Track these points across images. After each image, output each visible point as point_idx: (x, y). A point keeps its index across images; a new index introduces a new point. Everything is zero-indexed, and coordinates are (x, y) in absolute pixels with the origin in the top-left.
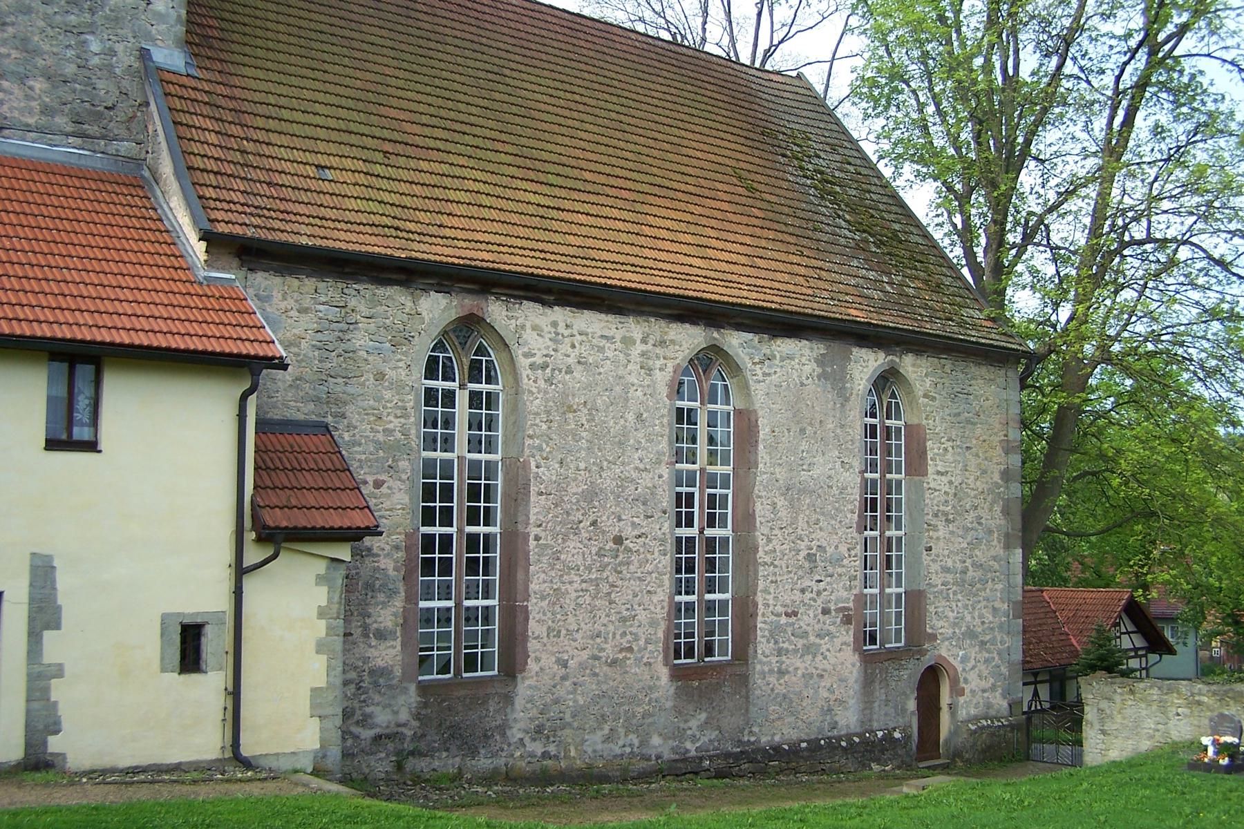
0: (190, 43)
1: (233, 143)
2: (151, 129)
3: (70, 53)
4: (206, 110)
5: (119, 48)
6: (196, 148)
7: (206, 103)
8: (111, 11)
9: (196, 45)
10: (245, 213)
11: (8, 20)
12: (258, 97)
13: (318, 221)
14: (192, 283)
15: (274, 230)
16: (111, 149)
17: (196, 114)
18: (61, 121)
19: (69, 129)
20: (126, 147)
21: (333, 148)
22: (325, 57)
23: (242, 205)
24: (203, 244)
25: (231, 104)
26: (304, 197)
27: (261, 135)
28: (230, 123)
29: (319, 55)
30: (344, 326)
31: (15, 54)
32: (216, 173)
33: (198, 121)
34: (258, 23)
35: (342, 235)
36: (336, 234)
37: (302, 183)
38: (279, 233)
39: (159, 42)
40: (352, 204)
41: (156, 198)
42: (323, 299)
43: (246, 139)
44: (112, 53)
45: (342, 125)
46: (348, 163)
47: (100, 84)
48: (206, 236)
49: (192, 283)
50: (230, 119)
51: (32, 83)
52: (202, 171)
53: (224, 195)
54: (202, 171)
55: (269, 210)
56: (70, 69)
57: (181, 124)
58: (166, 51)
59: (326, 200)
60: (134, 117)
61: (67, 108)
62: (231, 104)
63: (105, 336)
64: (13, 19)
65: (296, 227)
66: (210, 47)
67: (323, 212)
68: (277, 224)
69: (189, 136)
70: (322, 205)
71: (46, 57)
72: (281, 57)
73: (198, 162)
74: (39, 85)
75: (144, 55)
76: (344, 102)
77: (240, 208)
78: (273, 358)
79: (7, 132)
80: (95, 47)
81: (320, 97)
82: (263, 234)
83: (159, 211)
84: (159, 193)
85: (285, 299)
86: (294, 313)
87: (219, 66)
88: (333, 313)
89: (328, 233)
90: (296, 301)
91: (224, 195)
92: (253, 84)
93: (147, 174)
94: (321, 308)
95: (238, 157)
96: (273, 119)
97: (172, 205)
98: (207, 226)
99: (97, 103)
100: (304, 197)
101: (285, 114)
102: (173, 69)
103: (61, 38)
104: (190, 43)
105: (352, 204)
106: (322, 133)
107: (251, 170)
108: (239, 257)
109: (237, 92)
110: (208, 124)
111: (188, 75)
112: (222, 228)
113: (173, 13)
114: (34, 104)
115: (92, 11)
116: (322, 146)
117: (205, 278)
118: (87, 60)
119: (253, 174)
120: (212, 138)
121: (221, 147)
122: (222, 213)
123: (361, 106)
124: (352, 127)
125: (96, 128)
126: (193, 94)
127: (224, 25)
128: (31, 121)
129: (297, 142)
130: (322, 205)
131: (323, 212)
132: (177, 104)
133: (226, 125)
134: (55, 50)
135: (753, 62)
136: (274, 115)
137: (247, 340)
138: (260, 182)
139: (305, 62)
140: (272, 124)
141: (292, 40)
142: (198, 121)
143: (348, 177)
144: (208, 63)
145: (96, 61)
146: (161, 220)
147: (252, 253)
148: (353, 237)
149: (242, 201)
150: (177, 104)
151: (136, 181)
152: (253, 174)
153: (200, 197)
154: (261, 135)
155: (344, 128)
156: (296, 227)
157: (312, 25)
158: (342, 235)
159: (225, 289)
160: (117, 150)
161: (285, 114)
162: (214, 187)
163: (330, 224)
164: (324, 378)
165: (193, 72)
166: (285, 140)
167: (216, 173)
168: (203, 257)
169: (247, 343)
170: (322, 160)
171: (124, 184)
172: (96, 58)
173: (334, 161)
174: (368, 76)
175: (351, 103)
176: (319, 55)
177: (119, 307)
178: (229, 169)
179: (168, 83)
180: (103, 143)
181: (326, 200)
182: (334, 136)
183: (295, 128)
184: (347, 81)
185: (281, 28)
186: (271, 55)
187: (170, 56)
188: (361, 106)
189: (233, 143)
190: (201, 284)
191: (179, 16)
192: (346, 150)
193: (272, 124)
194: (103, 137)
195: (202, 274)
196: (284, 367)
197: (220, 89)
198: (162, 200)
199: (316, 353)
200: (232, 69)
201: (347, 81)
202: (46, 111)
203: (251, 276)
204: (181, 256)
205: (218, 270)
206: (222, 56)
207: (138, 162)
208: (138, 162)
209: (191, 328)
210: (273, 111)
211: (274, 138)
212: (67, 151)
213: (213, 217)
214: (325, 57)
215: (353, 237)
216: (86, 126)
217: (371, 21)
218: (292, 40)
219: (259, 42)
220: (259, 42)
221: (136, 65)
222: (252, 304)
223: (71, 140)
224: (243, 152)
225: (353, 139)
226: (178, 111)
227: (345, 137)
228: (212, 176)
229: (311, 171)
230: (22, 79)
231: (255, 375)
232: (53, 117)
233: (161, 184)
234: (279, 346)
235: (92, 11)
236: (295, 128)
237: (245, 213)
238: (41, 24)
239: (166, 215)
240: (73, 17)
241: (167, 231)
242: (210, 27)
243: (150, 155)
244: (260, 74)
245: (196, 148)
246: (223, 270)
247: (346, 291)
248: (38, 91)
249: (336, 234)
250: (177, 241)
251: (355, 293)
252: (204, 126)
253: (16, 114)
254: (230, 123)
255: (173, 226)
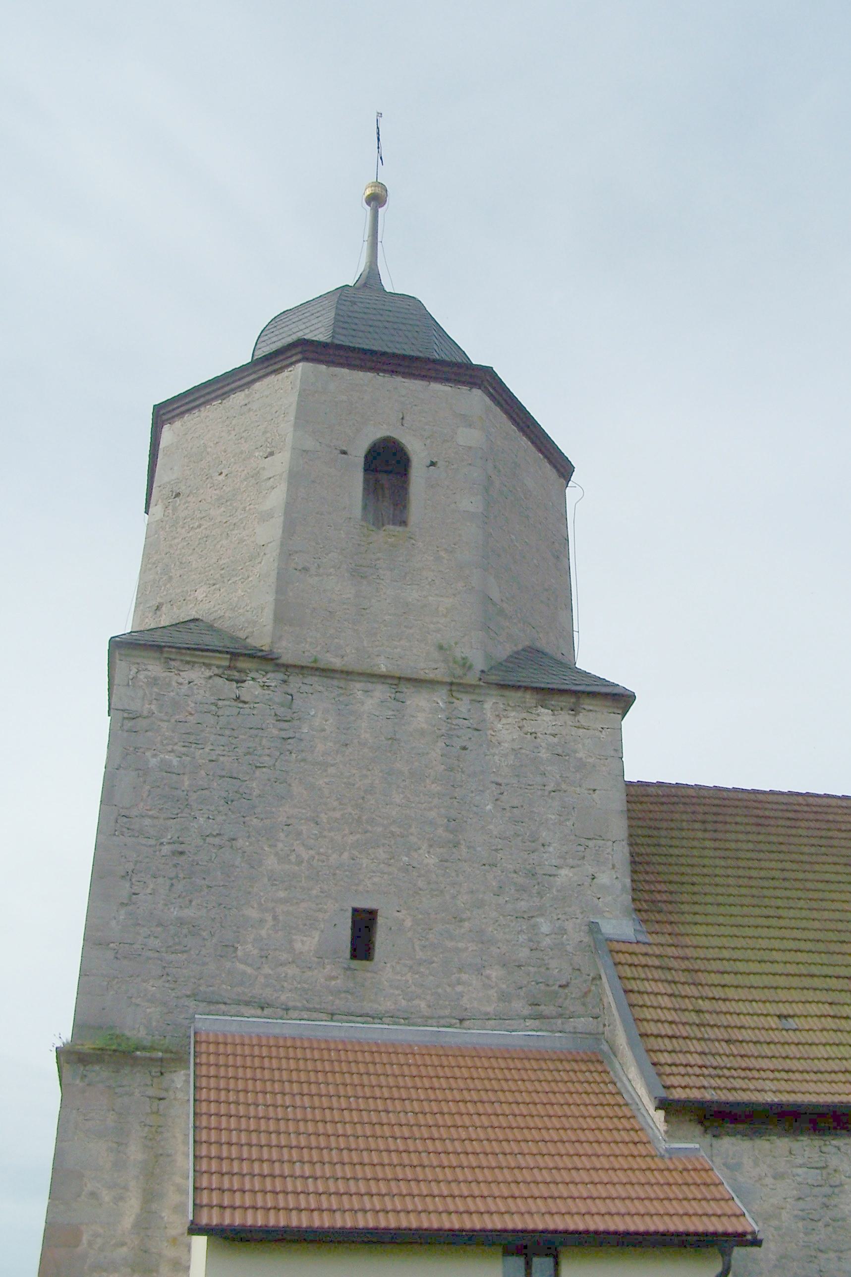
0: (640, 911)
1: (687, 1004)
2: (605, 1000)
3: (522, 938)
4: (658, 974)
5: (569, 925)
6: (648, 1014)
7: (657, 968)
8: (558, 891)
9: (646, 911)
10: (703, 1075)
11: (464, 916)
12: (711, 954)
13: (784, 1075)
14: (652, 1157)
15: (735, 1089)
16: (569, 1027)
17: (648, 980)
18: (519, 1006)
19: (526, 1011)
20: (582, 1023)
21: (795, 995)
22: (779, 903)
23: (700, 1067)
24: (661, 1114)
25: (685, 964)
26: (767, 1050)
27: (718, 992)
28: (683, 984)
29: (774, 902)
30: (827, 1190)
31: (472, 947)
32: (670, 1037)
33: (648, 986)
34: (707, 880)
35: (812, 1087)
36: (805, 1087)
37: (763, 1036)
38: (740, 1092)
39: (606, 914)
40: (821, 1052)
41: (615, 1072)
42: (800, 1161)
43: (702, 998)
44: (563, 931)
45: (803, 969)
46: (813, 1009)
47: (553, 964)
48: (663, 1104)
49: (652, 1157)
50: (683, 980)
51: (488, 972)
52: (657, 1036)
53: (681, 1058)
54: (657, 1036)
55: (729, 1069)
56: (523, 954)
57: (631, 991)
58: (614, 921)
59: (792, 1051)
60: (590, 991)
61: (522, 993)
62: (685, 964)
63: (558, 1223)
64: (468, 914)
65: (759, 1084)
66: (659, 912)
67: (788, 1064)
68: (738, 1083)
69: (641, 1003)
70: (787, 1057)
71: (500, 944)
72: (734, 910)
73: (652, 1028)
74: (495, 973)
75: (593, 928)
76: (802, 945)
77: (697, 1070)
78: (744, 1234)
79: (468, 1022)
80: (545, 928)
81: (777, 944)
82: (731, 1097)
83: (618, 1085)
84: (618, 1066)
85: (756, 1164)
86: (769, 1180)
87: (668, 928)
88: (813, 1176)
89: (796, 1086)
90: (770, 1166)
91: (681, 1058)
92: (703, 941)
93: (605, 1047)
94: (799, 1171)
95: (694, 1018)
96: (728, 973)
97: (630, 1077)
98: (663, 1093)
99: (551, 983)
100: (767, 1050)
101: (741, 967)
102: (624, 938)
103: (513, 924)
104: (640, 911)
105: (821, 1052)
106: (782, 981)
107: (708, 1029)
108: (701, 1123)
109: (690, 952)
110: (661, 988)
111: (638, 942)
112: (678, 1094)
113: (618, 885)
114: (492, 992)
115: (540, 894)
116: (782, 995)
117: (666, 1150)
118: (539, 942)
119: (711, 1033)
120: (665, 1001)
121: (675, 1010)
122: (679, 1077)
123: (821, 947)
124: (814, 970)
125: (552, 1008)
126: (643, 960)
127: (672, 888)
128: (490, 1009)
129: (756, 994)
130: (787, 1057)
131: (788, 1064)
132: (628, 972)
133: (679, 986)
134: (508, 937)
135: (226, 658)
136: (729, 969)
137: (696, 1214)
138: (718, 1040)
139: (757, 911)
140: (727, 979)
141: (743, 891)
142: (648, 986)
143: (814, 1023)
144: (657, 927)
145: (547, 941)
146: (619, 1093)
147: (719, 1118)
148: (825, 1087)
149: (700, 1063)
150: (628, 972)
151: (595, 1058)
152: (711, 1033)
153: (654, 1064)
154: (718, 992)
155: (805, 972)
156: (759, 1084)
157: (763, 874)
158: (812, 1087)
159: (690, 1161)
160: (575, 1028)
161: (741, 967)
162: (669, 1052)
163: (798, 1076)
164: (813, 1253)
165: (642, 938)
166: (742, 994)
167: (670, 1037)
168: (662, 1126)
169: (713, 1219)
170: (785, 1009)
171: (582, 1060)
172: (548, 939)
173: (798, 1009)
174: (826, 915)
175: (809, 946)
176: (774, 902)
177: (574, 1190)
178: (684, 1031)
179: (617, 952)
180: (559, 1021)
181: (792, 1051)
182: (795, 982)
183: (754, 980)
184: (804, 924)
185: (731, 881)
186: (722, 909)
187: (620, 926)
188: (821, 947)
189: (687, 1004)
190: (662, 1157)
191: (624, 886)
192: (810, 995)
193: (727, 979)
194: (560, 1016)
195: (663, 1146)
196: (756, 1243)
197: (671, 951)
198: (621, 1073)
199: (800, 1224)
200: (682, 929)
201: (804, 924)
202: (504, 997)
203: (715, 1142)
204: (642, 1129)
205: (680, 1139)
206: (672, 918)
207: (596, 1036)
208: (596, 1036)
209: (651, 1207)
210: (727, 966)
211: (731, 993)
212: (522, 1035)
213: (668, 1083)
214: (779, 903)
215: (825, 1087)
216: (542, 1007)
217: (823, 859)
218: (743, 891)
219: (709, 899)
220: (709, 899)
221: (586, 940)
222: (719, 1174)
223: (529, 1023)
224: (698, 1012)
225: (817, 982)
226: (628, 979)
227: (808, 982)
228: (667, 1041)
229: (773, 1022)
230: (479, 970)
231: (726, 1254)
232: (510, 1002)
233: (619, 1055)
234: (750, 1220)
235: (540, 894)
236: (754, 980)
237: (703, 1075)
238: (494, 914)
239: (626, 1088)
240: (523, 903)
241: (627, 1104)
242: (659, 892)
243: (607, 1027)
244: (712, 930)
245: (648, 1014)
246: (685, 1139)
247: (824, 1149)
248: (494, 979)
249: (805, 1087)
250: (637, 1113)
251: (834, 1150)
252: (656, 990)
253: (475, 1004)
254: (683, 984)
255: (633, 1099)
